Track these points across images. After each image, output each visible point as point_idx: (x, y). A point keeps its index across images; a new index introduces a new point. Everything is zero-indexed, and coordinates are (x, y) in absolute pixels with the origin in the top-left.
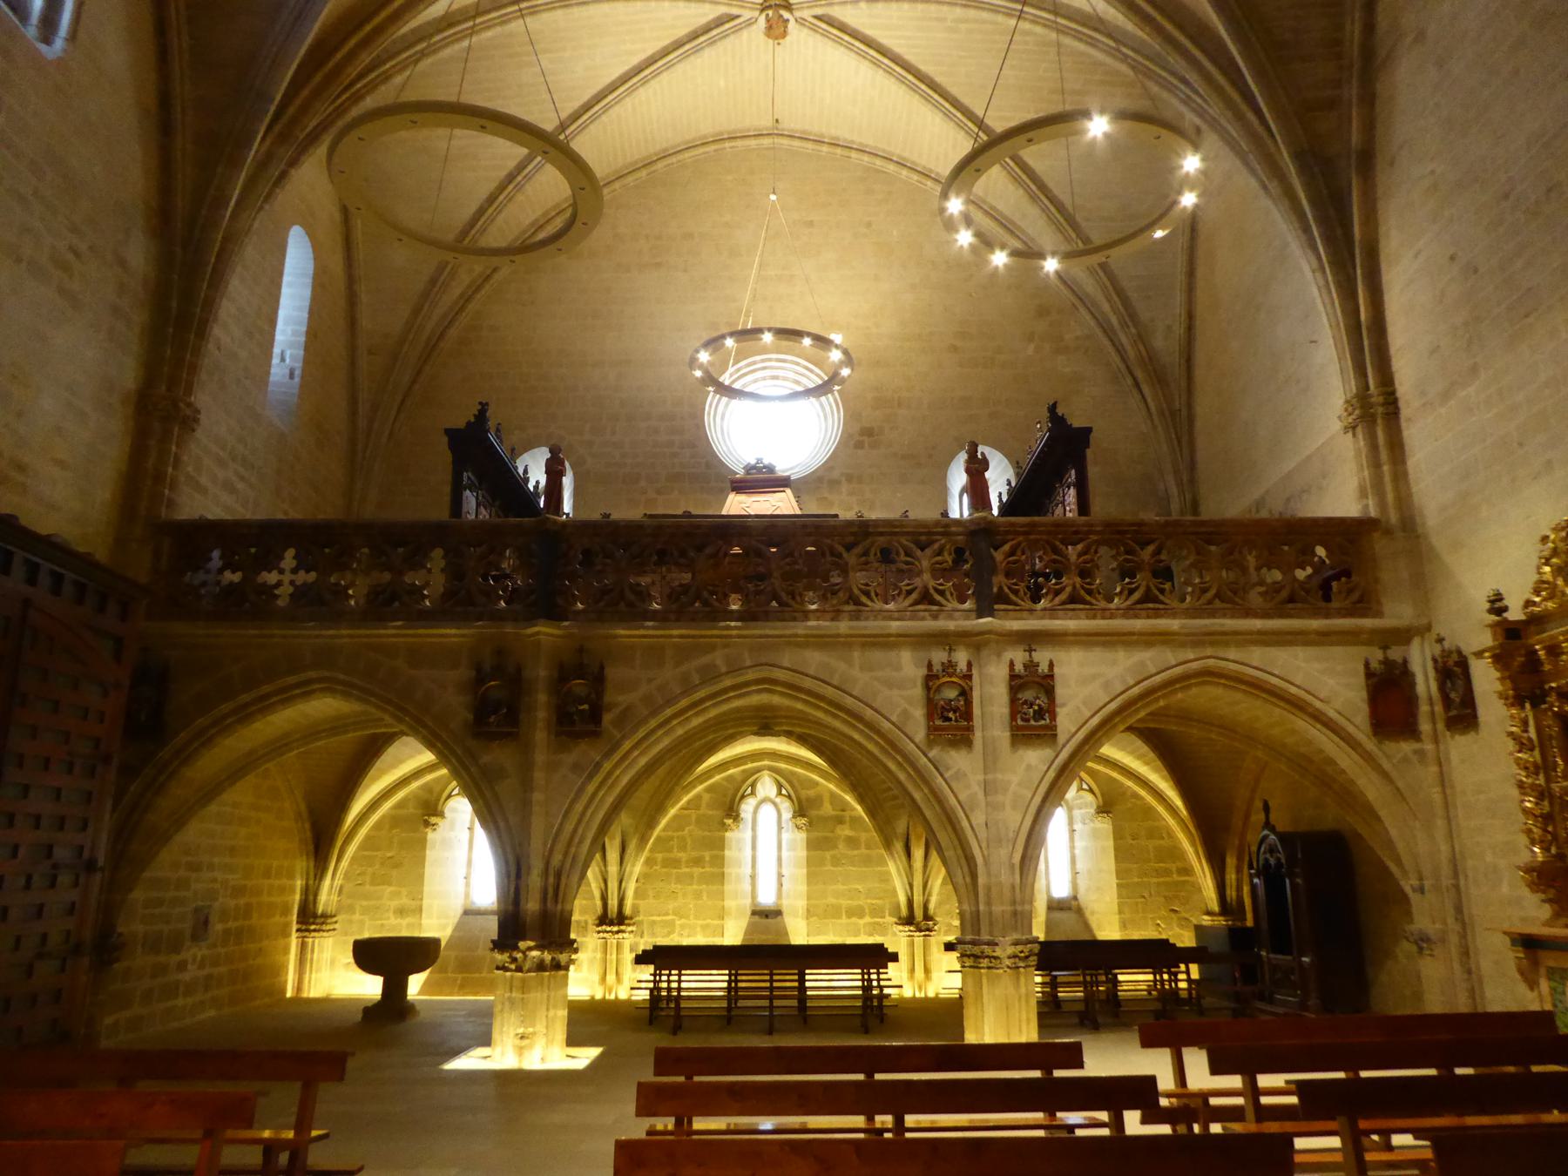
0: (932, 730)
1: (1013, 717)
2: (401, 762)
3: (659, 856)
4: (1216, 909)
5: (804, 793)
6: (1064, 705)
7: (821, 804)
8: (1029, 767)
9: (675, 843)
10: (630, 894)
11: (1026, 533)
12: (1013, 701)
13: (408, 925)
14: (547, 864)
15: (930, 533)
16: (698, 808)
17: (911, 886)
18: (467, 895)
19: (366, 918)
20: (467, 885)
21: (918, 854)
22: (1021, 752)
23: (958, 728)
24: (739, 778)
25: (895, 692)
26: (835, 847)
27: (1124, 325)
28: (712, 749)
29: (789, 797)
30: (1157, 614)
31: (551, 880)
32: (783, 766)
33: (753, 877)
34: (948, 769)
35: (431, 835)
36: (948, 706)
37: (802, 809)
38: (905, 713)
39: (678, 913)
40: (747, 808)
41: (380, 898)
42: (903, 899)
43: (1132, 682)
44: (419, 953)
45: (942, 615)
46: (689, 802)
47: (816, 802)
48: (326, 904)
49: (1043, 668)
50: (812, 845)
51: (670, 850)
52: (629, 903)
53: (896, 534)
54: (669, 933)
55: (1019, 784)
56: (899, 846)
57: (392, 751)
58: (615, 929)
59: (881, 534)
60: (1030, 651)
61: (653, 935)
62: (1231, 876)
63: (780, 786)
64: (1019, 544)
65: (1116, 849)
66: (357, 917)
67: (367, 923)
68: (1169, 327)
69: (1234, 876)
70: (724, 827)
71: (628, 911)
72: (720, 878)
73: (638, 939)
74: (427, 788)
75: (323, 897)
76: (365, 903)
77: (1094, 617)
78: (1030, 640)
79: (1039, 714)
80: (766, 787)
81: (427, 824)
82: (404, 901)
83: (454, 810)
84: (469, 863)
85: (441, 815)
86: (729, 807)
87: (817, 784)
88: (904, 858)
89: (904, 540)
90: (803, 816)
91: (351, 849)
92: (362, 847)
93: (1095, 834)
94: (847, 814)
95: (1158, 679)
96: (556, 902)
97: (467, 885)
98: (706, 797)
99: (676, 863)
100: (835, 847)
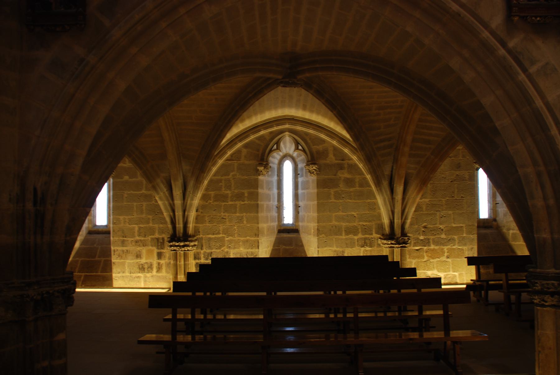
3: (212, 193)
5: (315, 148)
16: (239, 159)
21: (399, 189)
29: (304, 151)
32: (299, 128)
39: (227, 232)
42: (386, 221)
46: (232, 155)
47: (324, 154)
50: (321, 184)
54: (220, 247)
56: (385, 184)
58: (182, 244)
63: (297, 144)
70: (258, 173)
71: (191, 231)
72: (256, 208)
73: (199, 250)
86: (261, 156)
87: (324, 141)
88: (389, 193)
90: (314, 164)
98: (245, 151)
99: (224, 198)
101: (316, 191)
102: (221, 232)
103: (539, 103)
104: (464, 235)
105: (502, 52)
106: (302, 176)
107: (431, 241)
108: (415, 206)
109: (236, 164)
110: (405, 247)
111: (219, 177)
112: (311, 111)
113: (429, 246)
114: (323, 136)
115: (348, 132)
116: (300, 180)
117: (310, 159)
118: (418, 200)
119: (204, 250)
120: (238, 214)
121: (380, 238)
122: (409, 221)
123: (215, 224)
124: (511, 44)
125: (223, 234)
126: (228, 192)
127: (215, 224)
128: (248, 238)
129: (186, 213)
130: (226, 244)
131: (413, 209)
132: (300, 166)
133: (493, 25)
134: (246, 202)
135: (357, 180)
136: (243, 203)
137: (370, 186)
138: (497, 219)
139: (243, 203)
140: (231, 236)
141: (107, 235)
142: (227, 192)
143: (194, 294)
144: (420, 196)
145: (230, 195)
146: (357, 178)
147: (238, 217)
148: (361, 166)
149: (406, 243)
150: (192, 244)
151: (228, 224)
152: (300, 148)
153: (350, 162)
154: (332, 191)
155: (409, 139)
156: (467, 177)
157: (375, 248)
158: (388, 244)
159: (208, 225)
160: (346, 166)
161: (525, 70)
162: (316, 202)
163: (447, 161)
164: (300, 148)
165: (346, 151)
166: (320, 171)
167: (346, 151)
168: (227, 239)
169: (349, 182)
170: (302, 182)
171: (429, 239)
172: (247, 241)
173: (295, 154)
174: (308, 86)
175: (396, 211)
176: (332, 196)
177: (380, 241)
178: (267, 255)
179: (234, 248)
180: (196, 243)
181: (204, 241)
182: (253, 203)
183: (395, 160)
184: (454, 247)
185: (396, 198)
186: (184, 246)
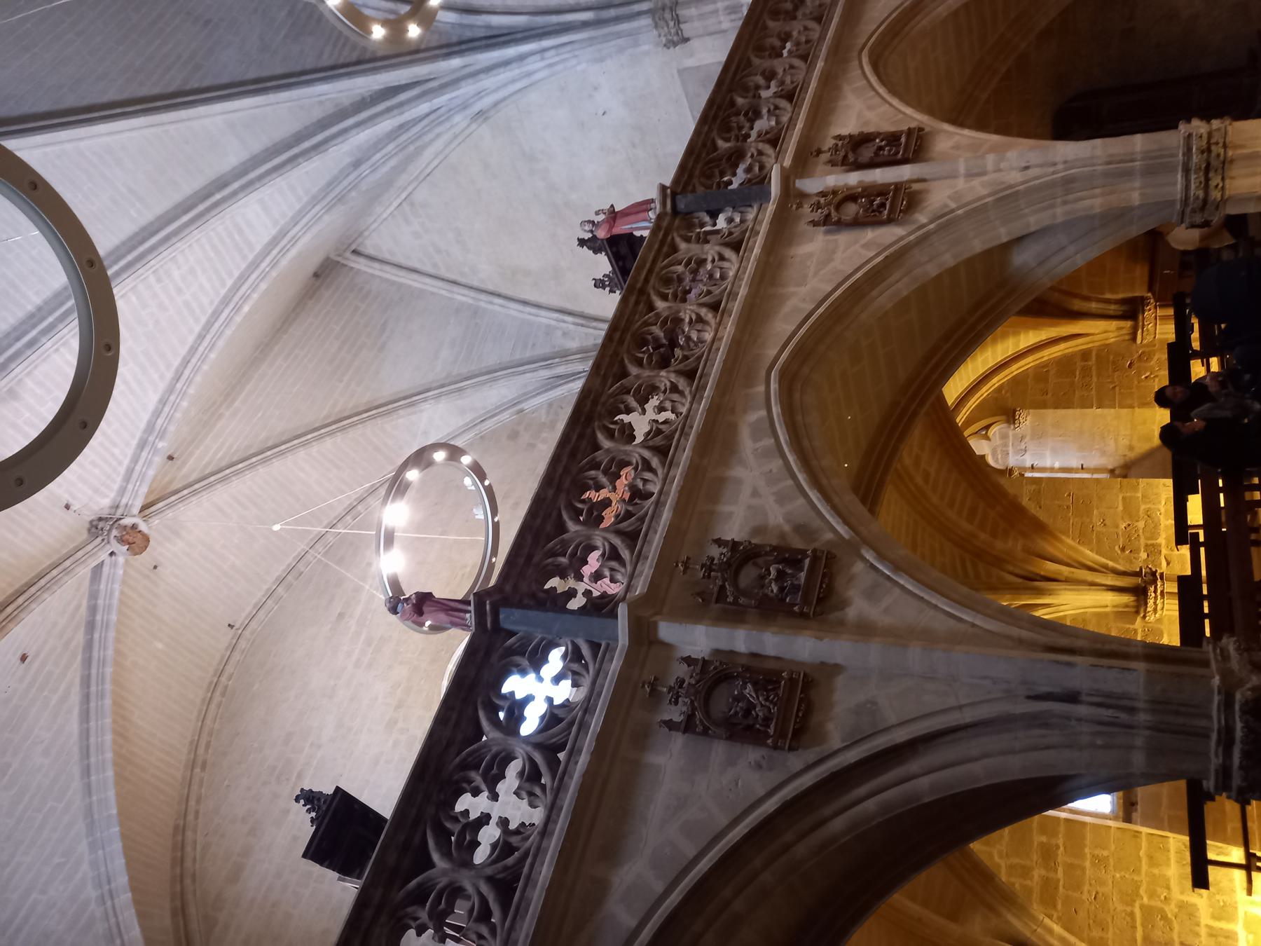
4: (1129, 324)
21: (1051, 567)
27: (548, 367)
36: (869, 208)
38: (866, 246)
39: (1130, 897)
42: (1110, 599)
53: (650, 271)
59: (647, 280)
62: (1094, 306)
65: (1057, 406)
68: (565, 334)
89: (660, 264)
93: (1039, 435)
99: (1049, 887)
102: (1129, 909)
104: (1139, 495)
107: (1150, 542)
110: (1162, 575)
113: (1160, 545)
117: (1003, 418)
121: (1144, 617)
122: (1111, 564)
123: (1109, 920)
125: (1132, 906)
127: (1109, 920)
128: (1142, 853)
130: (1159, 904)
134: (1061, 842)
136: (1062, 848)
138: (1110, 467)
139: (1062, 848)
140: (1138, 888)
142: (1036, 877)
143: (1206, 616)
145: (1043, 872)
147: (1093, 864)
149: (1154, 574)
156: (1034, 487)
157: (1164, 627)
158: (1156, 598)
159: (1110, 935)
168: (1145, 900)
171: (1146, 545)
172: (1150, 857)
177: (1151, 618)
179: (1168, 888)
182: (1062, 828)
184: (1163, 510)
185: (1066, 574)
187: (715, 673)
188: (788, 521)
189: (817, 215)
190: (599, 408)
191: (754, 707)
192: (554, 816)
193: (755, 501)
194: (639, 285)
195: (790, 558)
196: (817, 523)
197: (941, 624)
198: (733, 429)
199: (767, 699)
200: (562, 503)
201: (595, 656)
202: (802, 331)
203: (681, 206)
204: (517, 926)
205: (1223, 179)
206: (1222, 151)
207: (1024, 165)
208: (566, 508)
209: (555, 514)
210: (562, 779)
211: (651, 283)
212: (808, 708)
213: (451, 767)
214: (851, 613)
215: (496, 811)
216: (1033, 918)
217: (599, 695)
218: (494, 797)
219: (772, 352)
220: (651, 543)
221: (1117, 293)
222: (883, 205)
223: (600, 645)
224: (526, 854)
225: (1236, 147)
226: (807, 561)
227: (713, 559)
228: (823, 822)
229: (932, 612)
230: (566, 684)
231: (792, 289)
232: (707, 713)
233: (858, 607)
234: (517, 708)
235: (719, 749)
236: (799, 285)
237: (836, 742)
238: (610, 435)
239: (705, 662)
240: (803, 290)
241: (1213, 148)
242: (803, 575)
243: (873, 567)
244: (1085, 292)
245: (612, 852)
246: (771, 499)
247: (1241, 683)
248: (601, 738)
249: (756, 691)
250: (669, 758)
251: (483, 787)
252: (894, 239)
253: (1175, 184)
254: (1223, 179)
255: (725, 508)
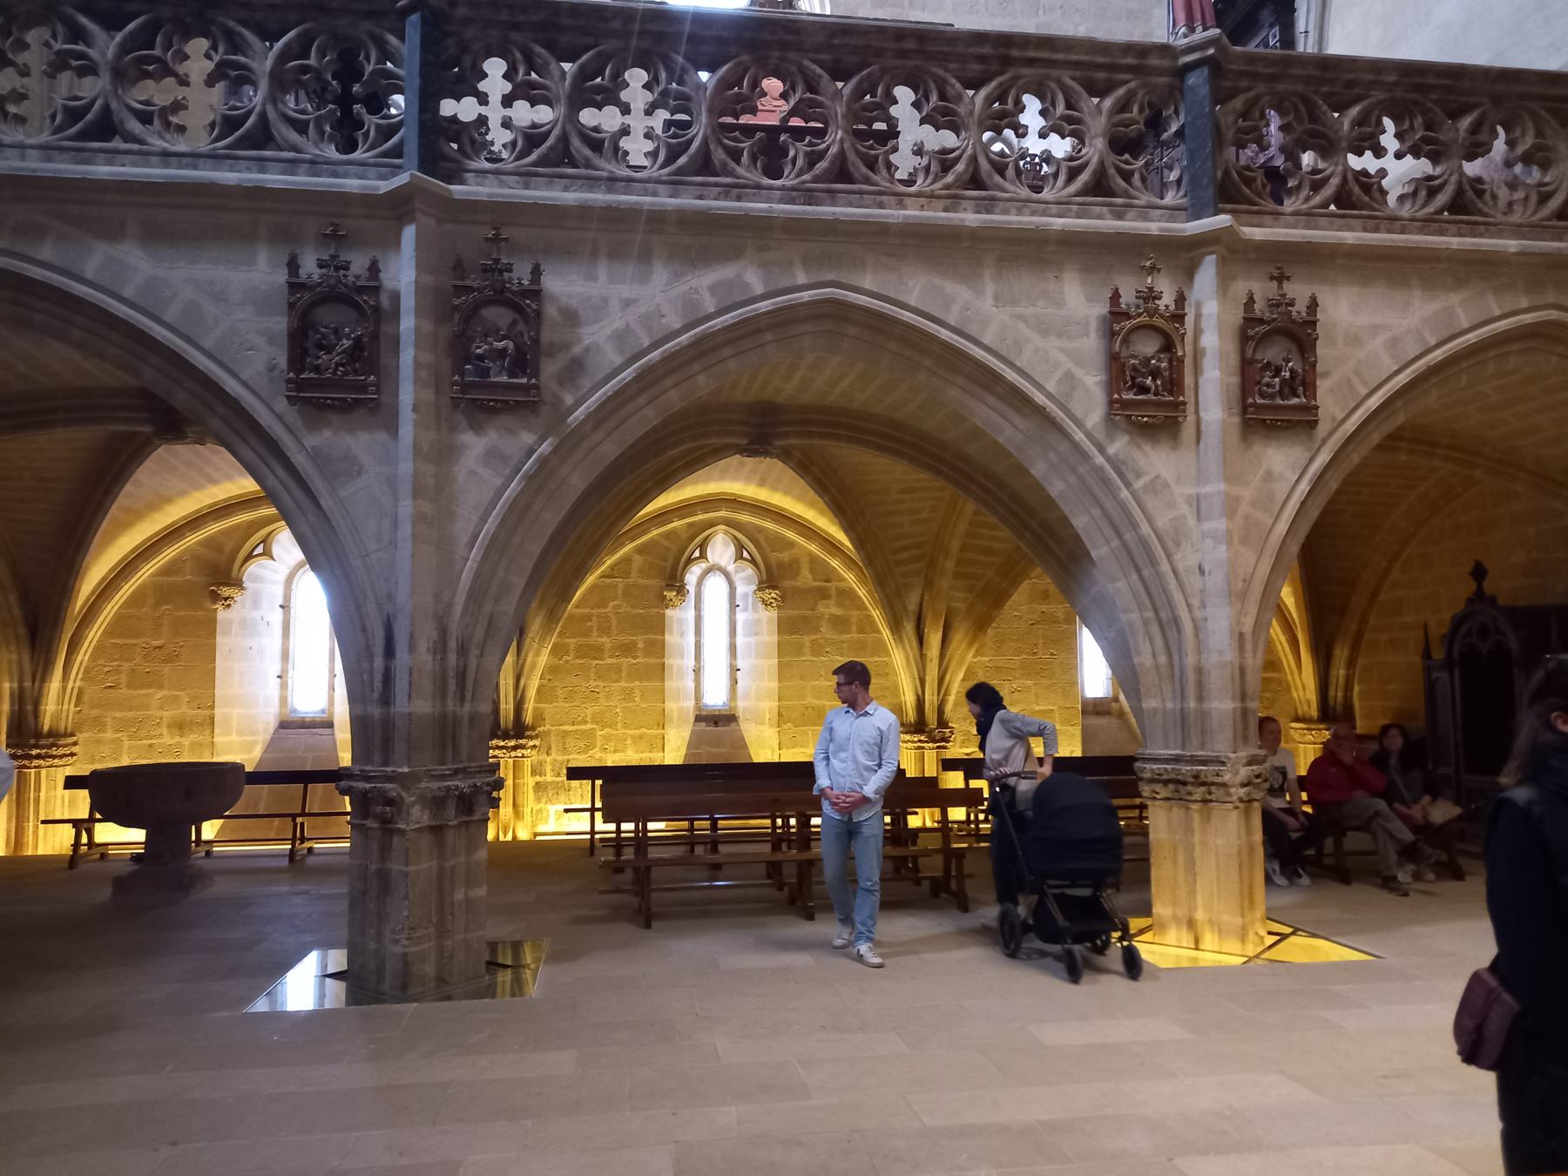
0: (1115, 406)
1: (1245, 391)
2: (168, 500)
3: (572, 642)
4: (1315, 713)
5: (775, 557)
6: (1326, 375)
7: (797, 573)
8: (1269, 477)
9: (594, 623)
10: (531, 693)
11: (1272, 78)
12: (1246, 364)
13: (193, 745)
14: (443, 632)
15: (1113, 68)
16: (627, 575)
17: (922, 681)
18: (283, 700)
19: (123, 736)
20: (284, 687)
21: (934, 639)
22: (1257, 448)
23: (1159, 405)
24: (684, 536)
25: (1055, 342)
26: (816, 630)
28: (664, 481)
29: (753, 561)
30: (1473, 229)
31: (452, 658)
32: (745, 518)
33: (697, 671)
34: (1138, 475)
35: (222, 614)
37: (772, 578)
39: (600, 720)
40: (691, 577)
41: (147, 707)
42: (909, 699)
43: (1433, 342)
44: (212, 786)
45: (1131, 214)
46: (612, 567)
47: (792, 568)
48: (57, 716)
49: (1300, 308)
50: (786, 627)
51: (587, 633)
52: (530, 707)
53: (1051, 63)
54: (588, 748)
55: (1253, 504)
56: (909, 627)
57: (147, 475)
58: (512, 743)
59: (1031, 62)
60: (1281, 279)
61: (564, 750)
62: (1339, 672)
63: (740, 547)
64: (1257, 99)
66: (109, 735)
67: (126, 744)
69: (1342, 672)
70: (664, 603)
71: (528, 718)
72: (660, 671)
73: (543, 757)
74: (212, 543)
75: (50, 706)
76: (119, 715)
77: (1376, 230)
78: (1280, 260)
79: (1290, 388)
80: (721, 550)
81: (215, 597)
82: (185, 710)
83: (257, 579)
84: (285, 655)
85: (239, 584)
86: (669, 574)
87: (791, 544)
88: (915, 643)
90: (774, 587)
91: (93, 635)
92: (110, 632)
94: (832, 585)
95: (1472, 337)
96: (462, 699)
97: (284, 687)
98: (638, 560)
99: (597, 652)
100: (816, 630)
101: (775, 638)
103: (1145, 529)
105: (1099, 460)
106: (745, 609)
108: (964, 669)
109: (620, 586)
111: (587, 611)
112: (774, 489)
114: (791, 535)
115: (846, 533)
116: (741, 617)
118: (969, 657)
119: (554, 756)
120: (624, 684)
122: (951, 699)
124: (1111, 450)
126: (605, 639)
129: (522, 682)
131: (961, 676)
132: (741, 589)
133: (1089, 425)
135: (854, 620)
137: (878, 631)
141: (327, 731)
144: (973, 650)
145: (608, 646)
146: (855, 615)
148: (862, 592)
150: (531, 743)
151: (602, 701)
152: (745, 554)
153: (842, 585)
154: (807, 639)
155: (955, 546)
160: (833, 592)
161: (1128, 485)
162: (776, 661)
163: (1025, 586)
164: (745, 554)
165: (834, 563)
166: (784, 601)
167: (834, 563)
169: (840, 624)
170: (746, 622)
172: (641, 737)
173: (731, 568)
174: (785, 455)
175: (928, 679)
176: (807, 650)
178: (679, 761)
180: (536, 742)
181: (553, 738)
182: (653, 661)
183: (929, 584)
186: (515, 748)
187: (364, 302)
188: (587, 350)
189: (1128, 298)
190: (776, 54)
191: (329, 352)
192: (185, 160)
193: (615, 305)
194: (1015, 53)
195: (524, 361)
196: (586, 384)
197: (461, 529)
198: (734, 254)
199: (337, 365)
200: (1379, 95)
201: (385, 155)
202: (907, 316)
203: (1193, 79)
204: (66, 155)
205: (1167, 799)
206: (1197, 797)
207: (1207, 570)
208: (599, 54)
209: (590, 41)
210: (228, 157)
211: (1025, 71)
212: (345, 408)
213: (221, 19)
214: (468, 438)
215: (638, 122)
216: (543, 639)
217: (336, 175)
218: (1399, 156)
219: (868, 283)
220: (549, 186)
221: (1360, 699)
222: (1144, 390)
223: (400, 156)
224: (141, 142)
225: (1207, 818)
226: (524, 380)
227: (510, 271)
228: (245, 441)
229: (475, 517)
230: (507, 136)
231: (990, 288)
232: (313, 305)
233: (474, 445)
234: (609, 96)
235: (280, 324)
236: (996, 298)
237: (311, 440)
238: (1475, 129)
239: (376, 290)
240: (987, 304)
241: (1203, 789)
242: (505, 379)
243: (531, 452)
244: (1361, 662)
245: (155, 236)
246: (618, 324)
247: (406, 788)
248: (258, 192)
249: (344, 352)
250: (263, 272)
251: (792, 103)
252: (1079, 414)
253: (1167, 748)
254: (1167, 799)
255: (602, 270)
